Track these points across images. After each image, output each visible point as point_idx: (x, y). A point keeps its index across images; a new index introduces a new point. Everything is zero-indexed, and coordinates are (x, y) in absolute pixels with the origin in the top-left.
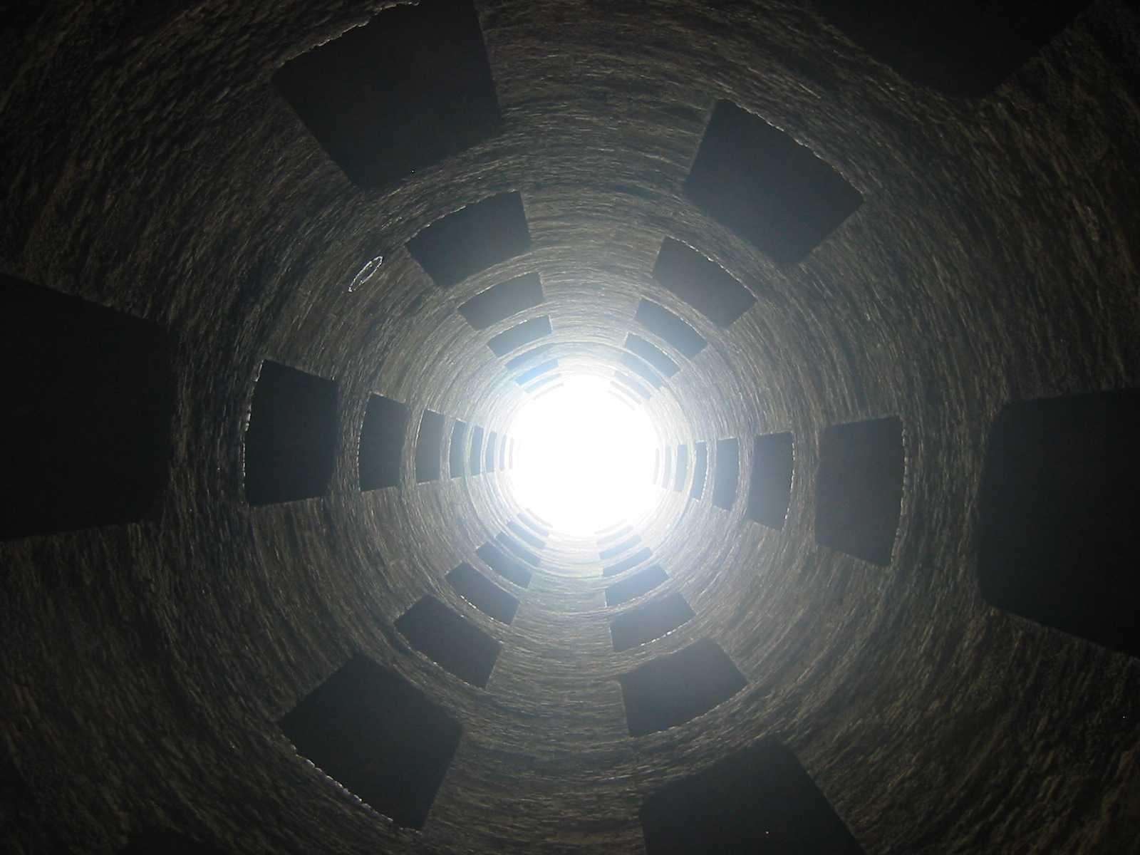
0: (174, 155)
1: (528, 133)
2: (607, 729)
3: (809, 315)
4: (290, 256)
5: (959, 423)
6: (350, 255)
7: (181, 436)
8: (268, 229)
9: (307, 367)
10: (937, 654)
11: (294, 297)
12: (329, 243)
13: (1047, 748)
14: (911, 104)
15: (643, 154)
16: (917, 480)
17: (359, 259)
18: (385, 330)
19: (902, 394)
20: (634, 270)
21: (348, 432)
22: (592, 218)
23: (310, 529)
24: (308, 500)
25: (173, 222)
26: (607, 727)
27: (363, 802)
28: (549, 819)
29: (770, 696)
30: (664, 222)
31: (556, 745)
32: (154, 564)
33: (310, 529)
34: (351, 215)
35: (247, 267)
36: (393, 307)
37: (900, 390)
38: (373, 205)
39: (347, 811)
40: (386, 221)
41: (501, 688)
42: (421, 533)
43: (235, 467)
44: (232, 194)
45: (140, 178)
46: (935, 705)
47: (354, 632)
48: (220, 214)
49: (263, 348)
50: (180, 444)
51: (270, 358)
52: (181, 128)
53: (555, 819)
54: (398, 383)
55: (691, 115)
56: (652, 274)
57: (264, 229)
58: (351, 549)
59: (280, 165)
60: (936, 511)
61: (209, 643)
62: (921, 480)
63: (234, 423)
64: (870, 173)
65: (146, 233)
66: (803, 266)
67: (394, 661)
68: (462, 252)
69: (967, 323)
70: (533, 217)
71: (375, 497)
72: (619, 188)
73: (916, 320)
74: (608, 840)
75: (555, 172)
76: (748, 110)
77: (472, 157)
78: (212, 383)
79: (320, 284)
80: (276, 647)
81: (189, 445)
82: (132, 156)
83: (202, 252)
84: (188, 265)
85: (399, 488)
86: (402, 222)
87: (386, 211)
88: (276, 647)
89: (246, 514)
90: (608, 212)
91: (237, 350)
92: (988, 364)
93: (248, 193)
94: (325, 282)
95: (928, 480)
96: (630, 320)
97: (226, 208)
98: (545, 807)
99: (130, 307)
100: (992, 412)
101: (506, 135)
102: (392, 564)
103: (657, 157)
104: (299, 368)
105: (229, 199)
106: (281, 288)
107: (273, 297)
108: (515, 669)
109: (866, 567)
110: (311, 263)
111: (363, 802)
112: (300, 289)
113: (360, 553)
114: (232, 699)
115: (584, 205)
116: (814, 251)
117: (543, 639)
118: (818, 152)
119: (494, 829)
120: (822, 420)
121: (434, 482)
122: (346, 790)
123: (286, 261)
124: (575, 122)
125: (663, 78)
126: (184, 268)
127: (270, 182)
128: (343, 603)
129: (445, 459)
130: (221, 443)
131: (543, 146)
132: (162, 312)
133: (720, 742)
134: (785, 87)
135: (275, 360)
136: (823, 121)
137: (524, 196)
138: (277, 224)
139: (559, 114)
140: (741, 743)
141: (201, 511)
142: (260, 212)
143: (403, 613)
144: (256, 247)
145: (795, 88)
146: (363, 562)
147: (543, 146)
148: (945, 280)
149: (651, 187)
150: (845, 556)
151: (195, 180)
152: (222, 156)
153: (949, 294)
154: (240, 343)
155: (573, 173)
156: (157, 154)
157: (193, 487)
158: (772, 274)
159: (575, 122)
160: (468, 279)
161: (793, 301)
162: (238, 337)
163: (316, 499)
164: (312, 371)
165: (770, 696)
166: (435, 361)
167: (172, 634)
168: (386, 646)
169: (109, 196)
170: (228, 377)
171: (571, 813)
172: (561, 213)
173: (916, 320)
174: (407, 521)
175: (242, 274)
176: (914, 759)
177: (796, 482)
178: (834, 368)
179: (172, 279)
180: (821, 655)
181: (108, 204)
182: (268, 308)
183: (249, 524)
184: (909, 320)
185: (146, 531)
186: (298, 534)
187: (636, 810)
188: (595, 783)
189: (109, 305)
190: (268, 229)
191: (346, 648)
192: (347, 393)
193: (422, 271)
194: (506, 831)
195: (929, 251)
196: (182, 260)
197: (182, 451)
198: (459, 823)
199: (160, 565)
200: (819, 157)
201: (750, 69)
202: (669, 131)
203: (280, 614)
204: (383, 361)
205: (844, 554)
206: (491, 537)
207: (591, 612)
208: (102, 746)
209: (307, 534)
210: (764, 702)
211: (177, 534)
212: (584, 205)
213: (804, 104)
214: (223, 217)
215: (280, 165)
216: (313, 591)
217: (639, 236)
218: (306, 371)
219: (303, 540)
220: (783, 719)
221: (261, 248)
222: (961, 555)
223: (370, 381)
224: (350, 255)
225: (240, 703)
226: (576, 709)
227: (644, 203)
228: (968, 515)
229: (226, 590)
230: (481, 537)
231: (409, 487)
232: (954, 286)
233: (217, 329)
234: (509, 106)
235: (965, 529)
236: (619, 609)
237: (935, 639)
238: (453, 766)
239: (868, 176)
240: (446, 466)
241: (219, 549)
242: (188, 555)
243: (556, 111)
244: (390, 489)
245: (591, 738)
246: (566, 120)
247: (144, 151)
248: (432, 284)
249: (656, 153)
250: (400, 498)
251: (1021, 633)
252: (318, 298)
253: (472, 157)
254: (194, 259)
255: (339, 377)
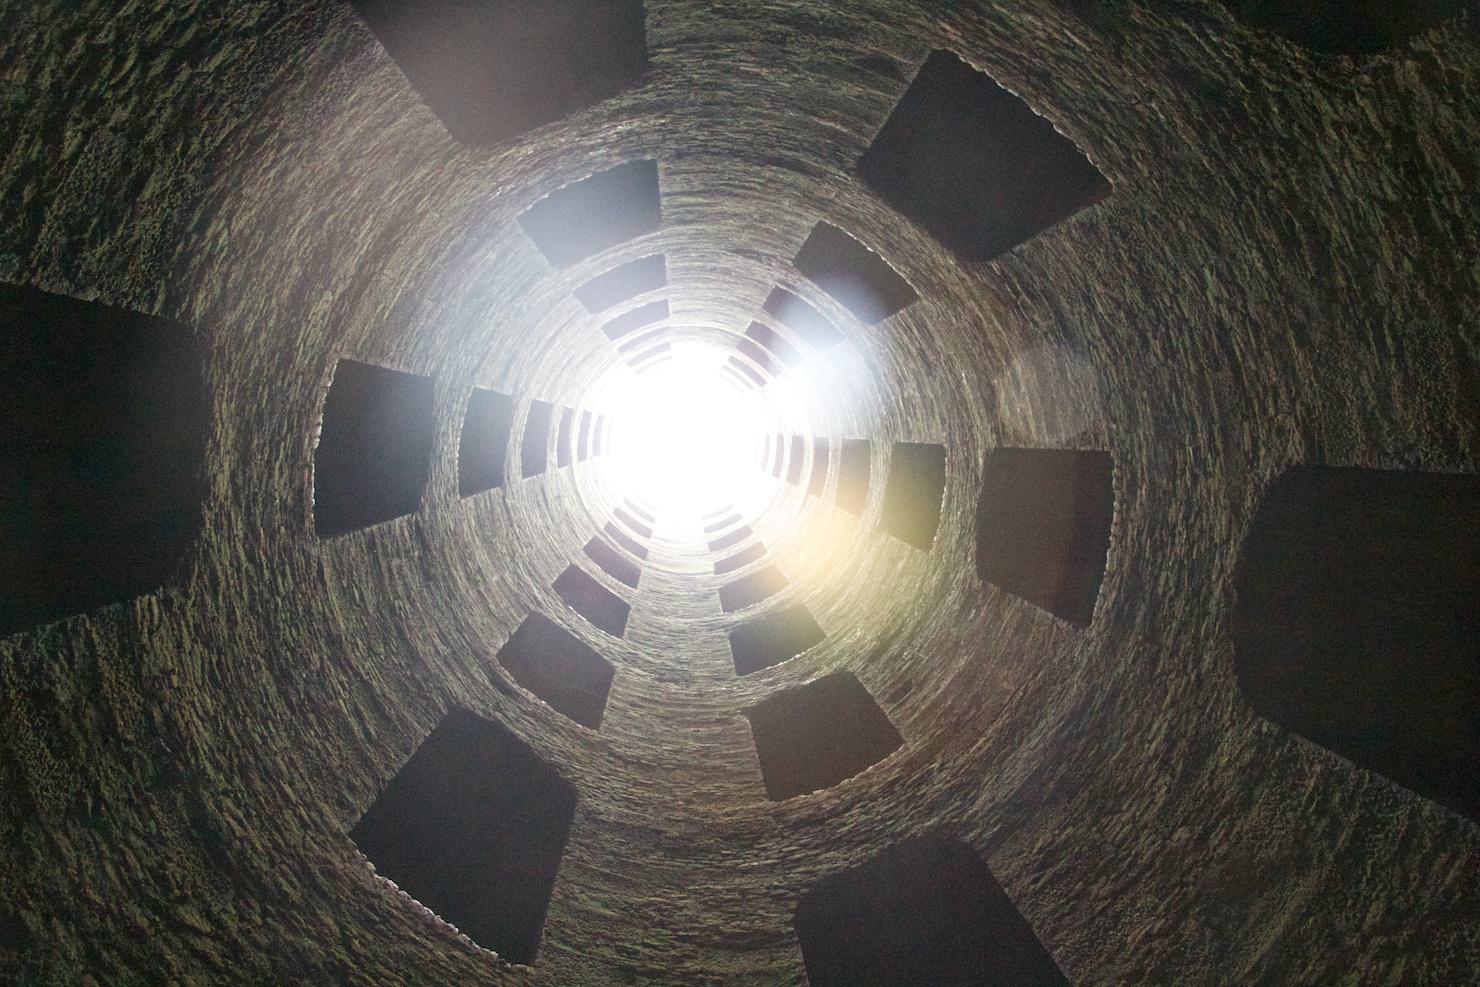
0: (183, 76)
1: (679, 85)
2: (740, 786)
3: (990, 322)
4: (371, 230)
5: (1207, 475)
6: (451, 229)
7: (221, 466)
8: (338, 194)
9: (395, 363)
10: (1177, 762)
11: (378, 281)
12: (423, 215)
13: (1390, 953)
14: (1239, 62)
15: (816, 119)
16: (1132, 532)
17: (463, 234)
18: (490, 318)
19: (1118, 427)
20: (773, 256)
21: (445, 434)
22: (737, 195)
23: (399, 556)
24: (397, 520)
25: (191, 178)
26: (742, 783)
27: (460, 932)
28: (686, 930)
29: (936, 765)
30: (822, 205)
31: (685, 810)
32: (179, 646)
33: (399, 556)
34: (452, 179)
35: (310, 243)
36: (500, 292)
37: (1115, 422)
38: (480, 168)
39: (440, 953)
40: (495, 189)
41: (617, 728)
42: (527, 536)
43: (300, 493)
44: (283, 142)
45: (126, 107)
46: (1182, 834)
47: (450, 677)
48: (266, 171)
49: (337, 345)
50: (220, 478)
51: (347, 357)
52: (189, 35)
53: (694, 929)
54: (505, 375)
55: (890, 69)
56: (793, 261)
57: (333, 194)
58: (448, 569)
59: (353, 105)
60: (1163, 575)
61: (258, 738)
62: (1140, 533)
63: (299, 441)
64: (1133, 157)
65: (147, 194)
66: (994, 265)
67: (498, 708)
68: (1032, 526)
69: (1243, 356)
70: (667, 190)
71: (476, 502)
72: (778, 162)
73: (1156, 345)
74: (761, 966)
75: (702, 138)
76: (974, 66)
77: (606, 113)
78: (266, 394)
79: (411, 265)
80: (352, 721)
81: (233, 475)
82: (106, 70)
83: (242, 223)
84: (221, 241)
85: (504, 488)
86: (515, 192)
87: (495, 177)
88: (352, 721)
89: (314, 552)
90: (755, 189)
91: (301, 349)
92: (1271, 411)
93: (306, 143)
94: (417, 263)
95: (1151, 535)
96: (757, 307)
97: (275, 161)
98: (681, 909)
99: (130, 299)
100: (1267, 471)
101: (650, 86)
102: (495, 578)
103: (832, 124)
104: (386, 365)
105: (279, 151)
106: (361, 268)
107: (348, 282)
108: (630, 699)
109: (1053, 622)
110: (400, 239)
111: (460, 932)
112: (385, 271)
113: (459, 573)
114: (288, 814)
115: (730, 179)
116: (1017, 249)
117: (659, 656)
118: (1061, 126)
119: (620, 950)
120: (989, 440)
121: (541, 475)
122: (438, 918)
123: (365, 237)
124: (739, 74)
125: (866, 16)
126: (215, 245)
127: (339, 128)
128: (437, 641)
129: (552, 450)
130: (281, 467)
131: (692, 104)
132: (184, 306)
133: (879, 821)
134: (1040, 33)
135: (354, 358)
136: (1083, 83)
137: (661, 165)
138: (351, 188)
139: (722, 61)
140: (908, 829)
141: (251, 557)
142: (327, 170)
143: (507, 640)
144: (323, 216)
145: (1056, 35)
146: (462, 582)
147: (692, 104)
148: (1218, 300)
149: (816, 162)
150: (1022, 603)
151: (221, 120)
152: (263, 85)
153: (1220, 320)
154: (304, 341)
155: (723, 140)
156: (152, 73)
157: (239, 529)
158: (949, 271)
159: (739, 74)
160: (587, 260)
161: (971, 304)
162: (302, 333)
163: (406, 517)
164: (403, 369)
165: (936, 765)
166: (682, 663)
167: (204, 737)
168: (487, 688)
169: (69, 133)
170: (289, 386)
171: (712, 919)
172: (702, 188)
173: (1156, 345)
174: (512, 525)
175: (305, 253)
176: (1162, 907)
177: (949, 502)
178: (1017, 386)
179: (196, 260)
180: (998, 724)
181: (69, 148)
182: (342, 296)
183: (320, 565)
184: (1145, 343)
185: (167, 603)
186: (384, 564)
187: (790, 916)
188: (734, 871)
189: (91, 299)
190: (338, 194)
191: (440, 702)
192: (445, 390)
193: (536, 249)
194: (636, 952)
195: (1201, 262)
196: (209, 233)
197: (223, 486)
198: (578, 947)
199: (187, 645)
200: (1060, 132)
201: (996, 6)
202: (857, 90)
203: (357, 674)
204: (487, 352)
205: (1019, 600)
206: (597, 529)
207: (706, 619)
208: (73, 954)
209: (395, 562)
210: (930, 772)
211: (215, 599)
212: (730, 179)
213: (1061, 59)
214: (272, 174)
215: (353, 105)
216: (401, 632)
217: (787, 218)
218: (395, 369)
219: (390, 570)
220: (958, 804)
221: (330, 219)
222: (1207, 638)
223: (473, 374)
224: (451, 229)
225: (301, 818)
226: (704, 756)
227: (802, 180)
228: (1217, 591)
229: (287, 660)
230: (589, 530)
231: (514, 485)
232: (1232, 309)
233: (271, 323)
234: (660, 46)
235: (1212, 606)
236: (737, 617)
237: (1171, 741)
238: (568, 853)
239: (1129, 161)
240: (552, 457)
241: (277, 605)
242: (232, 622)
243: (717, 57)
244: (493, 491)
245: (724, 798)
246: (727, 70)
247: (129, 64)
248: (547, 264)
249: (834, 119)
250: (504, 498)
251: (1318, 768)
252: (409, 282)
253: (606, 113)
254: (229, 234)
255: (437, 372)
